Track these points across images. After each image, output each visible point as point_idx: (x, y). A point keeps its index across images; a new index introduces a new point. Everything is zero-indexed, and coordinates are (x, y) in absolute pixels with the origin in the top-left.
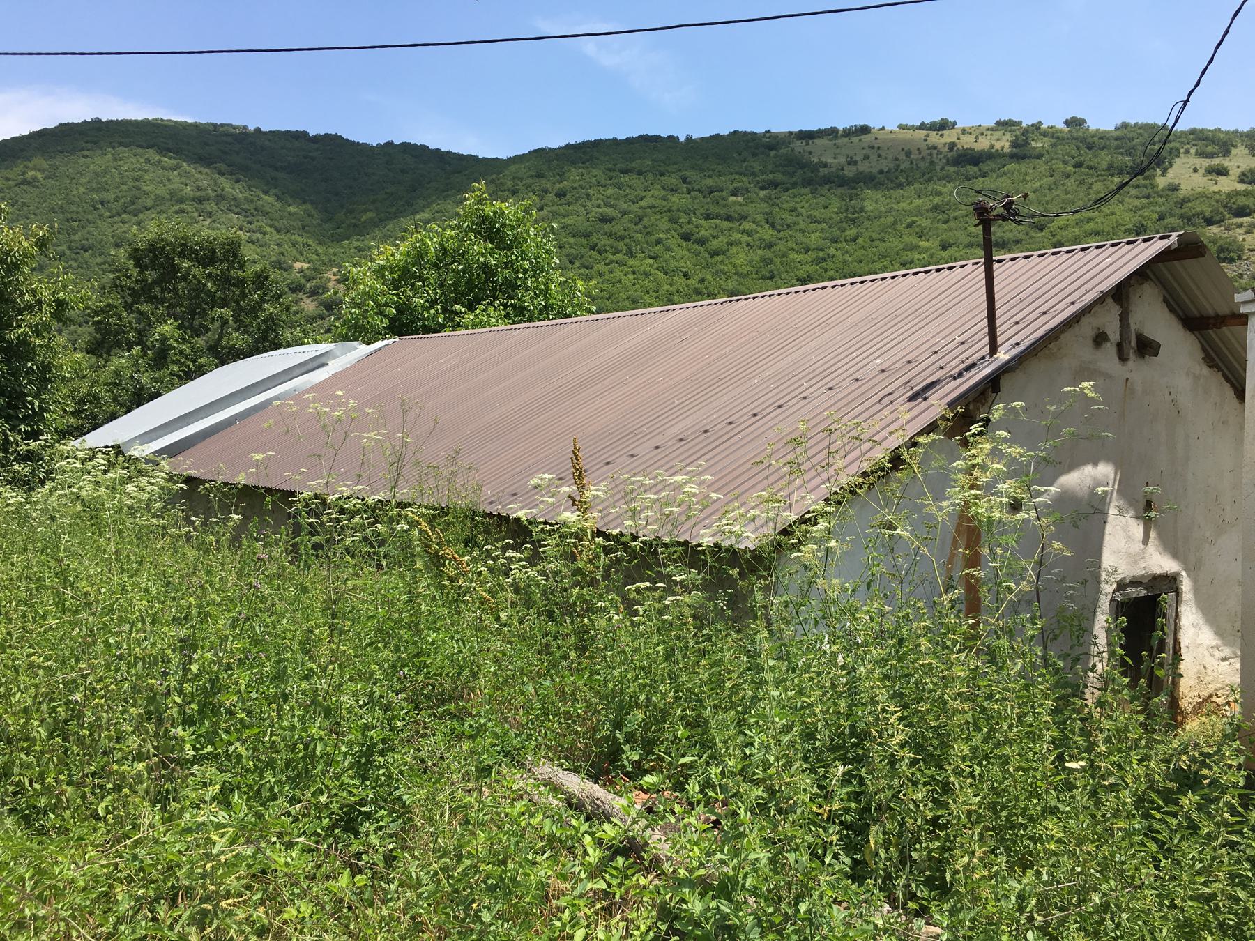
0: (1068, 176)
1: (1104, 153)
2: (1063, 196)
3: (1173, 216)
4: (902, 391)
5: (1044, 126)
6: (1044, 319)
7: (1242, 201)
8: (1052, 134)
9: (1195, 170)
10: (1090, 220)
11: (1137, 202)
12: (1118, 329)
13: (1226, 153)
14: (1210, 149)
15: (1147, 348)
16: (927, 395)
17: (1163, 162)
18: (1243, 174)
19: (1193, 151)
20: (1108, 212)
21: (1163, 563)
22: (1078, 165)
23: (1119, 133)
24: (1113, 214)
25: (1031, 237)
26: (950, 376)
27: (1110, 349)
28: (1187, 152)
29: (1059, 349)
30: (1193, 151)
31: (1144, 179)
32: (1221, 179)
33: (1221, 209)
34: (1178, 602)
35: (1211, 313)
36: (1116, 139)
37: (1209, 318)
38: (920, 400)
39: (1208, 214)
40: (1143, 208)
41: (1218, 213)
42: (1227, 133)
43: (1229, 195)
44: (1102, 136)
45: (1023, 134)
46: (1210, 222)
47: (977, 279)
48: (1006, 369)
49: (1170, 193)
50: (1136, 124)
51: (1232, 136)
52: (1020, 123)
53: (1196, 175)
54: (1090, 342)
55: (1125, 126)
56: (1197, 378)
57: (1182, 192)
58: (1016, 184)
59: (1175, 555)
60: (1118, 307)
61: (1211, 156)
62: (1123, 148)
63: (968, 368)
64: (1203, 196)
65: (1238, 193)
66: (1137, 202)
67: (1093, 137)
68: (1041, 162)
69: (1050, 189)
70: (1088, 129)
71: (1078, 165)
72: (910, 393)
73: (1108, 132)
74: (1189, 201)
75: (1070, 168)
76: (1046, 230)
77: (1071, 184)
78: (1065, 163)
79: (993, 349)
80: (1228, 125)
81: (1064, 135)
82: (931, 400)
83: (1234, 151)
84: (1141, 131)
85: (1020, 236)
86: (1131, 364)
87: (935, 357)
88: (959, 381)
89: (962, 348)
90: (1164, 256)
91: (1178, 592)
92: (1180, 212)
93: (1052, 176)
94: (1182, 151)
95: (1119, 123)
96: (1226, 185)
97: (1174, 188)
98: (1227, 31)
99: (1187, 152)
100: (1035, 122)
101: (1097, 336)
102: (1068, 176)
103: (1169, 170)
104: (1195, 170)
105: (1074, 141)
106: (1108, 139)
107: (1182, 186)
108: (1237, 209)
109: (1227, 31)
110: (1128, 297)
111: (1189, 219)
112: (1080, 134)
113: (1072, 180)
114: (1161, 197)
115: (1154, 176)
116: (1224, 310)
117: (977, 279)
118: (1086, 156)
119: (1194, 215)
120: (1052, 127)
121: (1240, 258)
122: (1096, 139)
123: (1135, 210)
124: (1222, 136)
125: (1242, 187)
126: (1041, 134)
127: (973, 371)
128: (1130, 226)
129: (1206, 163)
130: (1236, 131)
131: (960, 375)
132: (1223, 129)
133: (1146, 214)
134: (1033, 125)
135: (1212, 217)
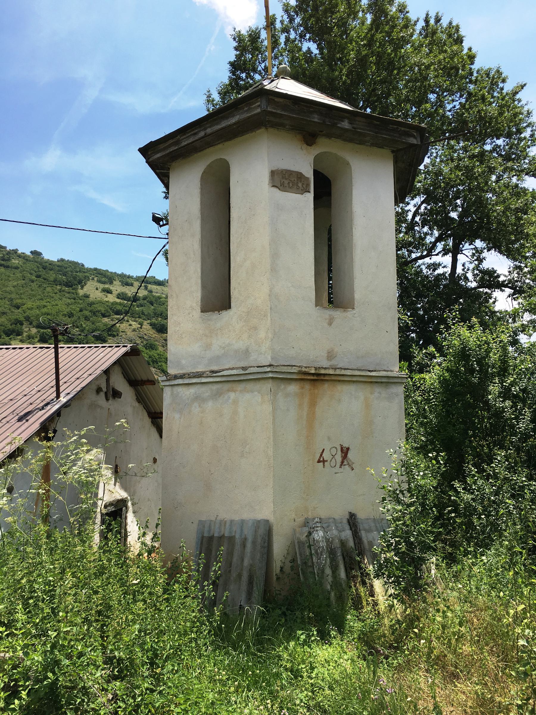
0: (33, 282)
1: (51, 272)
2: (31, 292)
3: (87, 310)
4: (11, 416)
5: (20, 252)
6: (78, 382)
7: (119, 308)
8: (22, 256)
9: (97, 289)
10: (45, 306)
11: (69, 301)
12: (105, 386)
13: (111, 283)
14: (103, 279)
15: (116, 394)
16: (28, 418)
17: (82, 283)
18: (119, 294)
19: (96, 279)
20: (54, 304)
21: (124, 494)
22: (38, 276)
23: (59, 264)
24: (57, 305)
25: (12, 312)
26: (38, 409)
27: (102, 394)
28: (93, 279)
29: (83, 395)
30: (96, 279)
31: (72, 289)
32: (109, 295)
33: (109, 310)
34: (126, 512)
35: (140, 379)
36: (58, 266)
37: (138, 381)
38: (24, 421)
39: (103, 312)
40: (71, 304)
41: (108, 312)
42: (111, 273)
43: (112, 304)
44: (51, 263)
45: (7, 254)
46: (104, 316)
47: (47, 360)
48: (66, 405)
49: (85, 298)
50: (68, 260)
51: (114, 275)
52: (5, 248)
53: (97, 291)
54: (95, 392)
55: (62, 260)
56: (134, 407)
57: (91, 299)
58: (3, 281)
59: (126, 490)
60: (105, 376)
61: (104, 283)
62: (61, 271)
63: (47, 405)
64: (101, 302)
65: (116, 303)
66: (69, 301)
67: (46, 263)
68: (18, 271)
69: (23, 287)
70: (43, 258)
71: (38, 276)
72: (17, 417)
73: (54, 262)
74: (94, 304)
75: (34, 278)
76: (20, 309)
77: (34, 285)
78: (31, 274)
79: (58, 396)
80: (112, 269)
81: (30, 259)
82: (31, 421)
83: (114, 282)
84: (70, 264)
85: (5, 310)
86: (110, 401)
87: (25, 398)
88: (43, 411)
89: (39, 394)
90: (126, 354)
91: (127, 508)
92: (90, 308)
93: (24, 280)
94: (90, 278)
95: (59, 258)
96: (111, 298)
97: (87, 296)
98: (151, 266)
99: (93, 279)
100: (15, 248)
101: (98, 389)
102: (33, 282)
103: (85, 287)
104: (97, 289)
105: (36, 263)
106: (54, 265)
107: (91, 296)
108: (116, 311)
109: (151, 266)
110: (109, 373)
111: (94, 313)
112: (39, 260)
113: (35, 284)
114: (81, 300)
115: (77, 289)
116: (145, 378)
117: (47, 360)
118: (43, 273)
119: (97, 311)
120: (24, 253)
121: (118, 335)
122: (47, 264)
123: (68, 305)
124: (109, 274)
125: (118, 301)
126: (18, 256)
127: (49, 407)
128: (65, 313)
129: (101, 286)
130: (116, 273)
131: (43, 408)
132: (110, 271)
133: (73, 307)
134: (13, 250)
135: (105, 313)
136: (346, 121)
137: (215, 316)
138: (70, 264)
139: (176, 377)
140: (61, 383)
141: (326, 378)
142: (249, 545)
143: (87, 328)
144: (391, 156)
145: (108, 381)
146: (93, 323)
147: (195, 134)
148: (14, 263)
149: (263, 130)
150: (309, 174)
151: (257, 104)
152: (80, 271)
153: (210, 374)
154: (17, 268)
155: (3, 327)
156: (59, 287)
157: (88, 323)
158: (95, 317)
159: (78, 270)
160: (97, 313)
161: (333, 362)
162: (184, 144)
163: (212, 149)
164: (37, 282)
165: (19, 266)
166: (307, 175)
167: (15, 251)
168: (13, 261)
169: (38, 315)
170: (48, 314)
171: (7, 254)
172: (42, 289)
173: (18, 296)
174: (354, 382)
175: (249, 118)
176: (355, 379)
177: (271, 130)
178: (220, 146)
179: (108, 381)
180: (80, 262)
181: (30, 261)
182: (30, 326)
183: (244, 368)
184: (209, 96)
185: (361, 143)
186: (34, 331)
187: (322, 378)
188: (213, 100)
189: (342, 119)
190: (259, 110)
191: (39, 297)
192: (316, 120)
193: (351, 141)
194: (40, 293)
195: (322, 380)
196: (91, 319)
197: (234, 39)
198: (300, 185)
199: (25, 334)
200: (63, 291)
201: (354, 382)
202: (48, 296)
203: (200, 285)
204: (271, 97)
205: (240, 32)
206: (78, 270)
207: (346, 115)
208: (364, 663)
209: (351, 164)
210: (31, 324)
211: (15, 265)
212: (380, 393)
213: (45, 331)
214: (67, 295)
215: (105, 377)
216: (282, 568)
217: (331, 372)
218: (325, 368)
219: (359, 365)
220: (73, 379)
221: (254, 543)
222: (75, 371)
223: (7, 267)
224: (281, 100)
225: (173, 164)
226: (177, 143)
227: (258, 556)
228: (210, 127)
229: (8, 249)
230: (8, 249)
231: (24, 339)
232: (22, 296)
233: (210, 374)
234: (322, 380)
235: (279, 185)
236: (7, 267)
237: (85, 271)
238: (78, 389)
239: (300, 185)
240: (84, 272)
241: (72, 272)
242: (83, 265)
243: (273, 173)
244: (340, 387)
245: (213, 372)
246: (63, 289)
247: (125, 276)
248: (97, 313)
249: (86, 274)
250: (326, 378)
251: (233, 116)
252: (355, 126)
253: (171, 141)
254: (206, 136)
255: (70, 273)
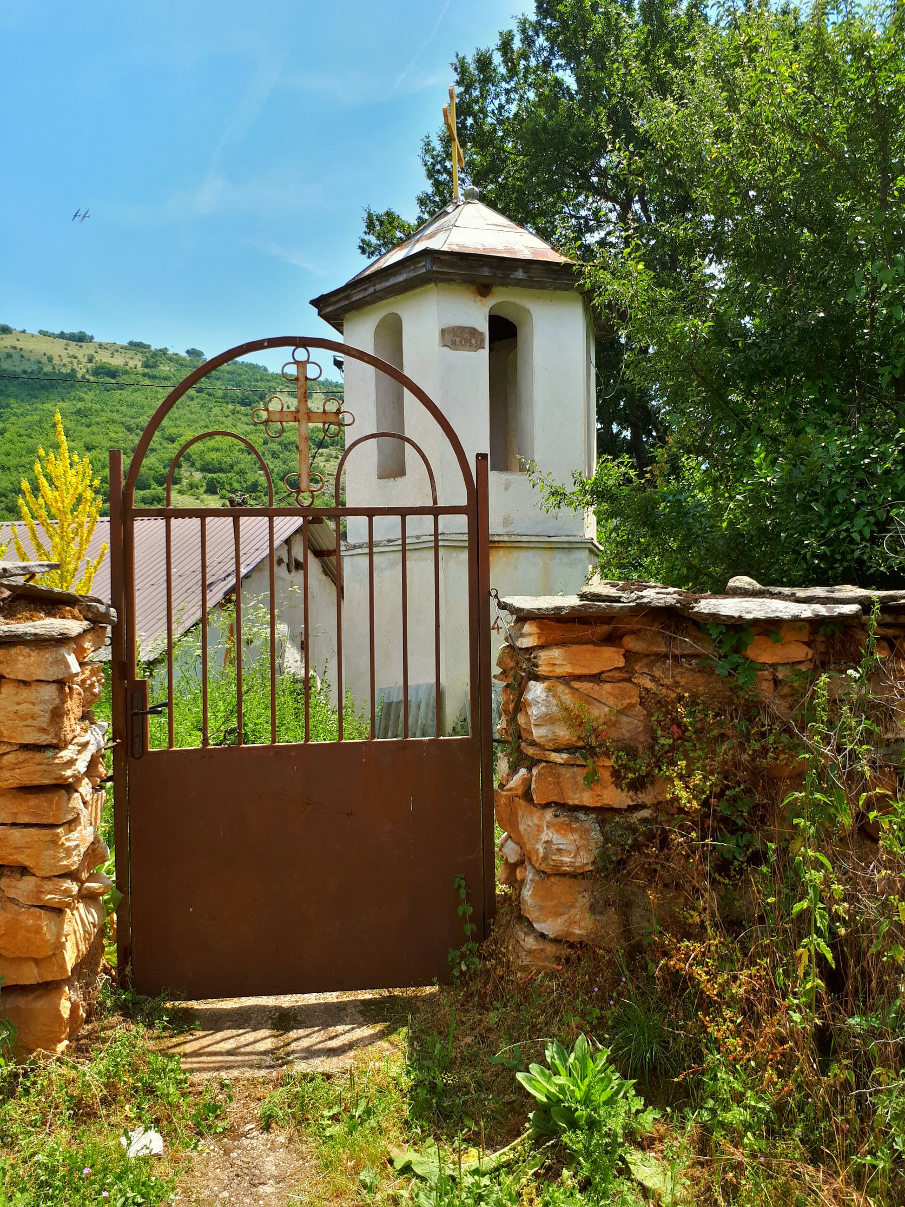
5: (170, 352)
8: (174, 359)
25: (164, 448)
40: (252, 433)
45: (152, 357)
52: (149, 347)
56: (320, 581)
84: (246, 369)
88: (225, 582)
100: (162, 347)
111: (286, 447)
113: (195, 402)
119: (289, 443)
120: (176, 355)
126: (168, 359)
134: (160, 350)
136: (520, 270)
137: (391, 482)
138: (246, 369)
139: (355, 547)
140: (241, 553)
141: (501, 545)
142: (423, 706)
143: (276, 470)
144: (581, 297)
145: (289, 551)
146: (284, 463)
147: (365, 289)
148: (163, 371)
149: (433, 285)
150: (483, 326)
151: (423, 263)
152: (261, 380)
153: (387, 543)
154: (167, 378)
155: (152, 472)
156: (231, 407)
157: (277, 462)
158: (288, 453)
159: (259, 378)
160: (290, 447)
161: (510, 529)
162: (355, 299)
163: (384, 302)
164: (199, 400)
165: (171, 375)
166: (480, 329)
167: (164, 352)
168: (162, 367)
169: (203, 452)
170: (217, 450)
171: (152, 357)
172: (206, 410)
173: (171, 423)
174: (532, 548)
175: (415, 276)
176: (532, 545)
177: (440, 285)
178: (392, 299)
179: (289, 551)
180: (261, 365)
181: (186, 366)
182: (192, 469)
183: (418, 537)
184: (428, 144)
185: (542, 288)
186: (198, 476)
187: (496, 545)
188: (434, 150)
189: (515, 269)
190: (424, 270)
191: (203, 423)
192: (486, 274)
193: (530, 287)
194: (204, 416)
195: (497, 547)
196: (281, 455)
197: (456, 69)
198: (473, 341)
199: (185, 482)
200: (238, 412)
201: (532, 548)
202: (215, 422)
203: (376, 450)
204: (436, 256)
205: (464, 58)
206: (259, 378)
207: (520, 263)
208: (59, 390)
209: (531, 310)
210: (193, 465)
211: (164, 374)
212: (561, 559)
213: (215, 476)
214: (244, 419)
215: (286, 547)
216: (454, 728)
217: (506, 538)
218: (499, 535)
219: (538, 530)
220: (252, 550)
221: (427, 705)
222: (255, 542)
223: (154, 377)
224: (447, 257)
225: (347, 315)
226: (348, 297)
227: (430, 715)
228: (380, 283)
229: (153, 348)
230: (153, 348)
231: (185, 489)
232: (178, 422)
233: (387, 543)
234: (497, 547)
235: (450, 344)
236: (154, 377)
237: (270, 378)
238: (258, 560)
239: (473, 341)
240: (268, 381)
241: (249, 381)
242: (265, 370)
243: (443, 331)
244: (516, 554)
245: (389, 541)
246: (238, 409)
247: (331, 383)
248: (290, 447)
249: (270, 384)
250: (501, 545)
251: (401, 274)
252: (530, 275)
253: (342, 295)
254: (375, 292)
255: (247, 383)
